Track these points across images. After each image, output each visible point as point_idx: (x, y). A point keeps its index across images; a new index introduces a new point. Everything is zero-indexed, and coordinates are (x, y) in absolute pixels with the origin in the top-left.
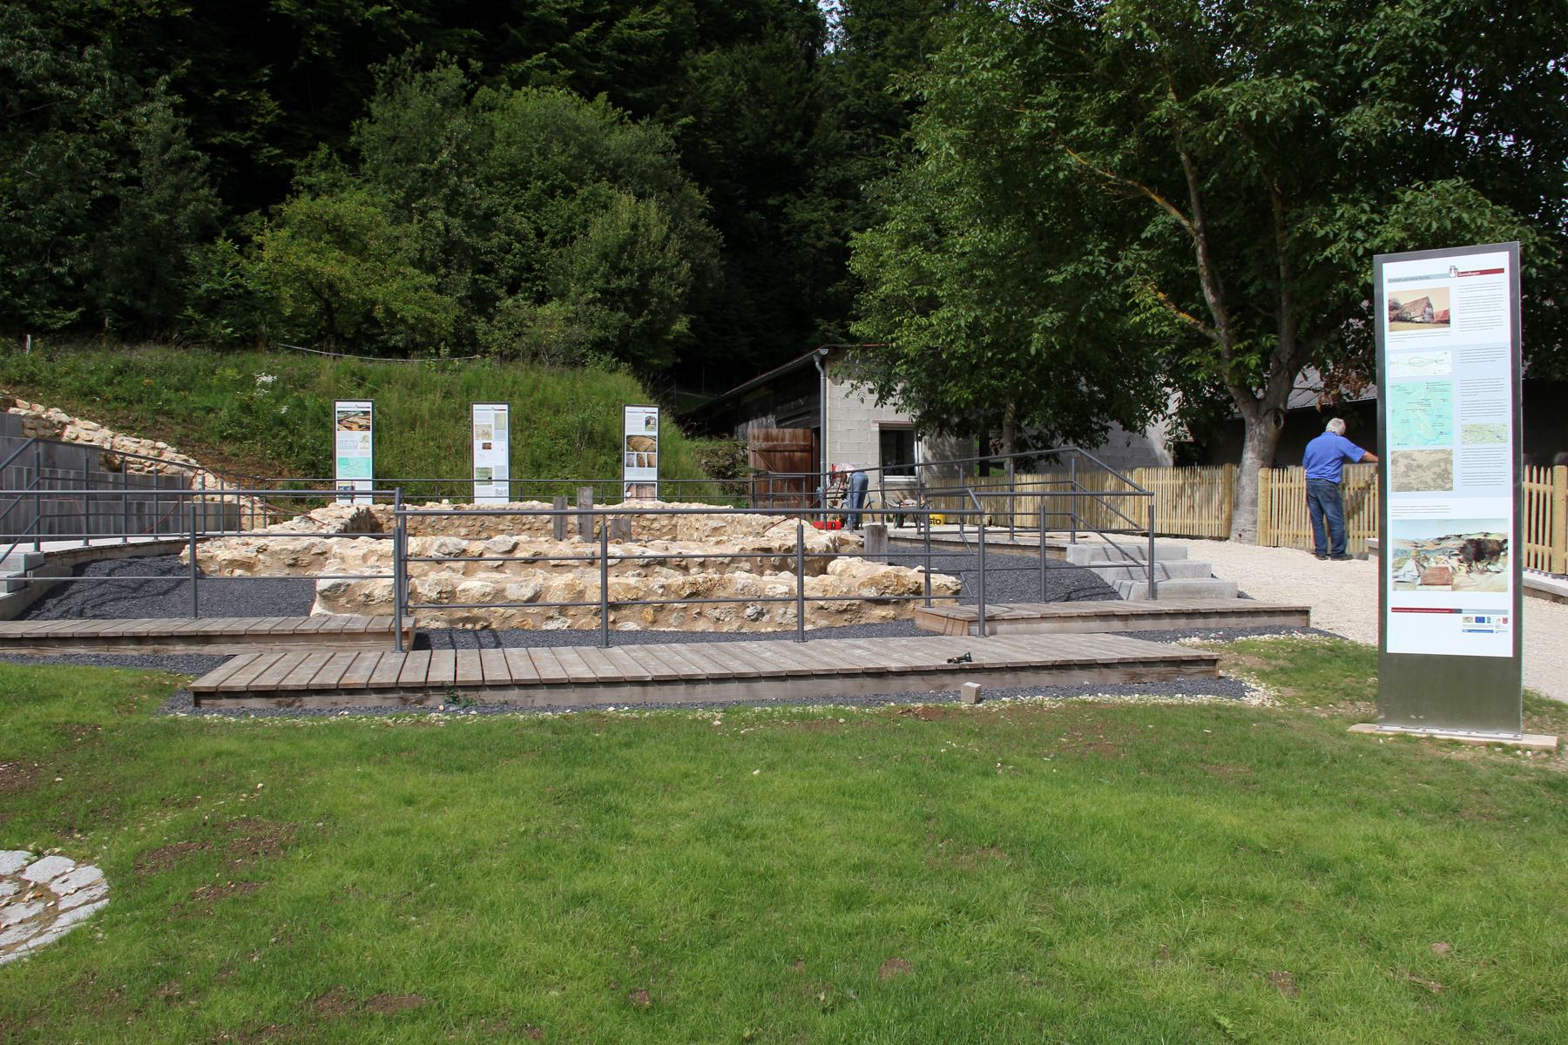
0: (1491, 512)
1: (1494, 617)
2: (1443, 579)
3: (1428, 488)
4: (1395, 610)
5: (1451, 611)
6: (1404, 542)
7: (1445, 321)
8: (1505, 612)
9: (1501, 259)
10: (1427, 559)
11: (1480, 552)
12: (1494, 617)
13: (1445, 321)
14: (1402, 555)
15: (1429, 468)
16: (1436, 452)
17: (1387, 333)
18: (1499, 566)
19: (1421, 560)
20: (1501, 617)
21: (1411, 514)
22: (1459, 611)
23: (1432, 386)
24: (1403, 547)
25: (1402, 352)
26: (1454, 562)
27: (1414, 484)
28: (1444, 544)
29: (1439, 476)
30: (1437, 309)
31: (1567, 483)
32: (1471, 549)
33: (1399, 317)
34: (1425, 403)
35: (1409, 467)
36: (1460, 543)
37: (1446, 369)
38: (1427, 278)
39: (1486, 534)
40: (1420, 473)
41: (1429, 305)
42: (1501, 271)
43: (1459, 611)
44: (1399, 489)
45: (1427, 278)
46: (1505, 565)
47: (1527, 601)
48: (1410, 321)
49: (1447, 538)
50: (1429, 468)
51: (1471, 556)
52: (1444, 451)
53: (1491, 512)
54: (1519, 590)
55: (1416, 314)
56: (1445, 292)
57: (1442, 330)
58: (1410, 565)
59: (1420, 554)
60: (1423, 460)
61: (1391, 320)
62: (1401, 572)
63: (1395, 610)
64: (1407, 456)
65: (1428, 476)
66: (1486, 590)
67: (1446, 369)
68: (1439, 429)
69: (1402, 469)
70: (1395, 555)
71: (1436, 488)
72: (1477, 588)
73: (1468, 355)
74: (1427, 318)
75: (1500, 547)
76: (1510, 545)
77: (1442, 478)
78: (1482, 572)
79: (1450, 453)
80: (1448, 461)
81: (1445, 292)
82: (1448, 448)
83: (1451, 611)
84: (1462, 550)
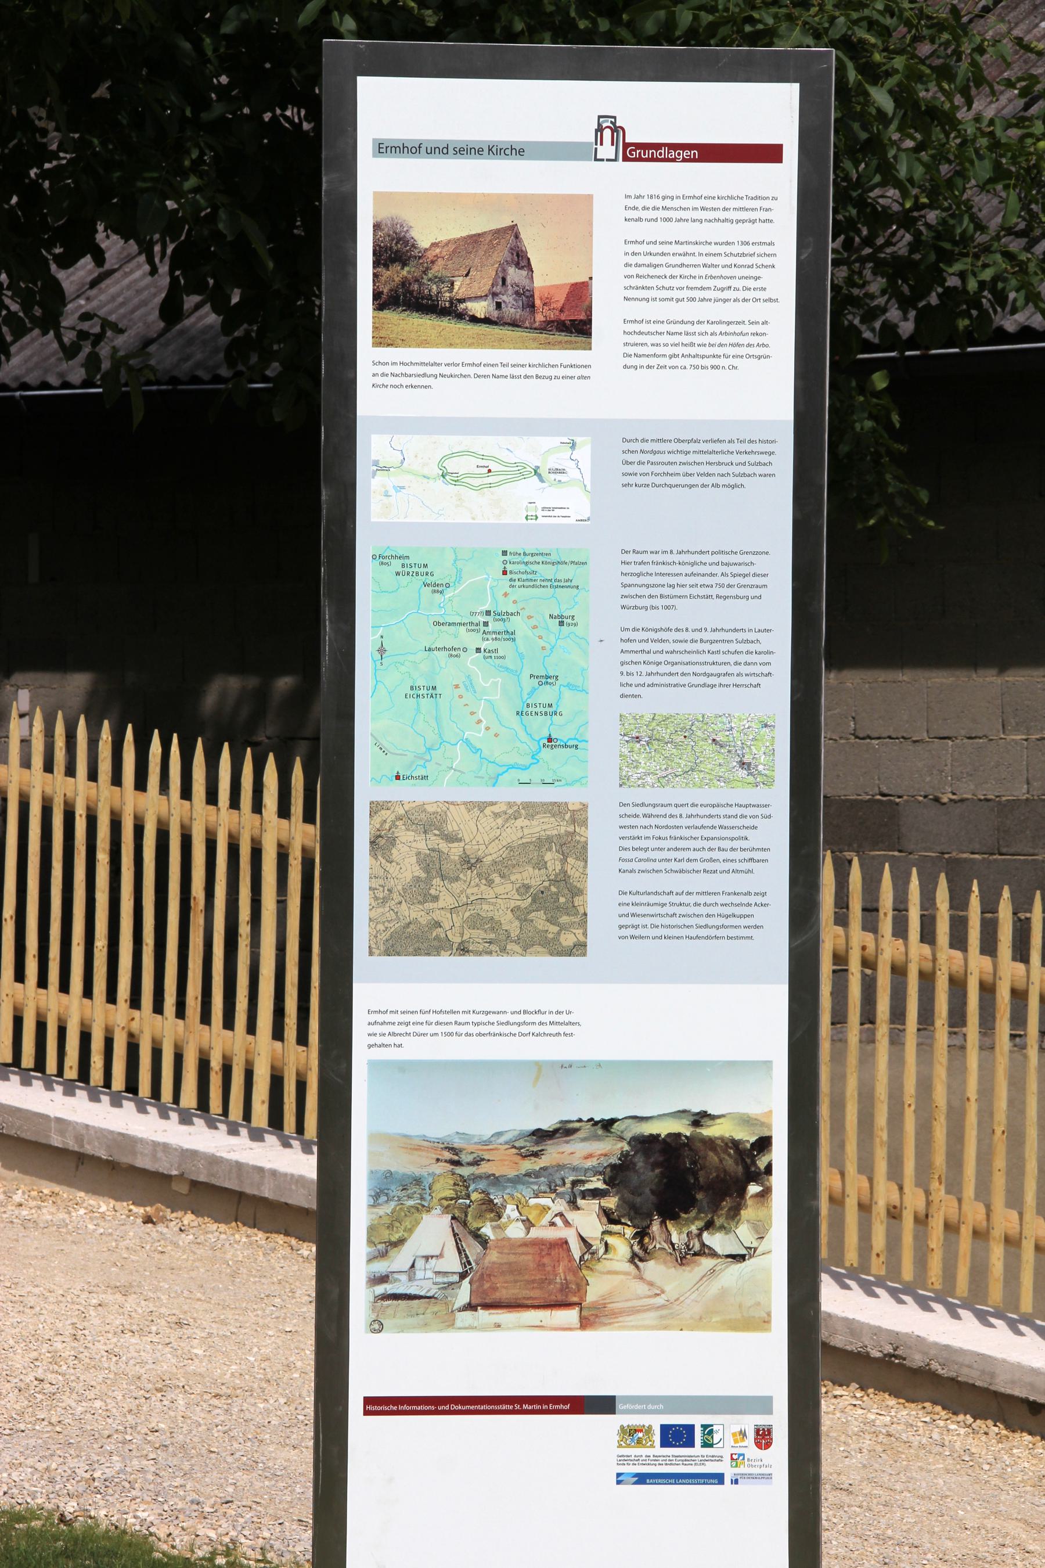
0: (699, 1025)
1: (726, 1426)
2: (548, 1284)
3: (499, 943)
4: (375, 1405)
5: (579, 1405)
6: (412, 1145)
7: (573, 324)
8: (764, 1405)
9: (769, 109)
10: (494, 1210)
11: (676, 1182)
12: (726, 1426)
13: (573, 324)
14: (403, 1193)
15: (503, 868)
16: (531, 810)
17: (367, 354)
18: (744, 1232)
19: (472, 1208)
20: (750, 1422)
21: (437, 1036)
22: (604, 1405)
23: (522, 566)
24: (405, 1165)
25: (430, 439)
26: (587, 1220)
27: (452, 927)
28: (554, 1153)
29: (540, 899)
30: (549, 274)
31: (970, 728)
32: (647, 1174)
33: (415, 294)
34: (493, 626)
35: (432, 865)
36: (611, 1149)
37: (575, 503)
38: (516, 151)
39: (700, 1119)
40: (469, 886)
41: (520, 259)
42: (771, 153)
43: (604, 1405)
44: (408, 941)
45: (516, 151)
46: (761, 1231)
47: (841, 1408)
48: (452, 311)
49: (565, 1131)
50: (503, 868)
51: (646, 1198)
52: (556, 809)
53: (699, 1025)
54: (816, 1358)
55: (473, 289)
56: (579, 207)
57: (563, 355)
58: (433, 1232)
59: (468, 1186)
60: (482, 837)
61: (382, 302)
62: (400, 1260)
63: (375, 1405)
64: (430, 822)
65: (501, 900)
66: (699, 1323)
67: (575, 503)
68: (541, 726)
69: (406, 867)
70: (377, 1196)
71: (526, 947)
72: (668, 1316)
73: (652, 459)
74: (512, 309)
75: (747, 1160)
76: (779, 1156)
77: (548, 916)
78: (684, 1257)
79: (578, 817)
80: (573, 847)
81: (579, 207)
82: (569, 796)
83: (579, 1405)
84: (617, 1174)
